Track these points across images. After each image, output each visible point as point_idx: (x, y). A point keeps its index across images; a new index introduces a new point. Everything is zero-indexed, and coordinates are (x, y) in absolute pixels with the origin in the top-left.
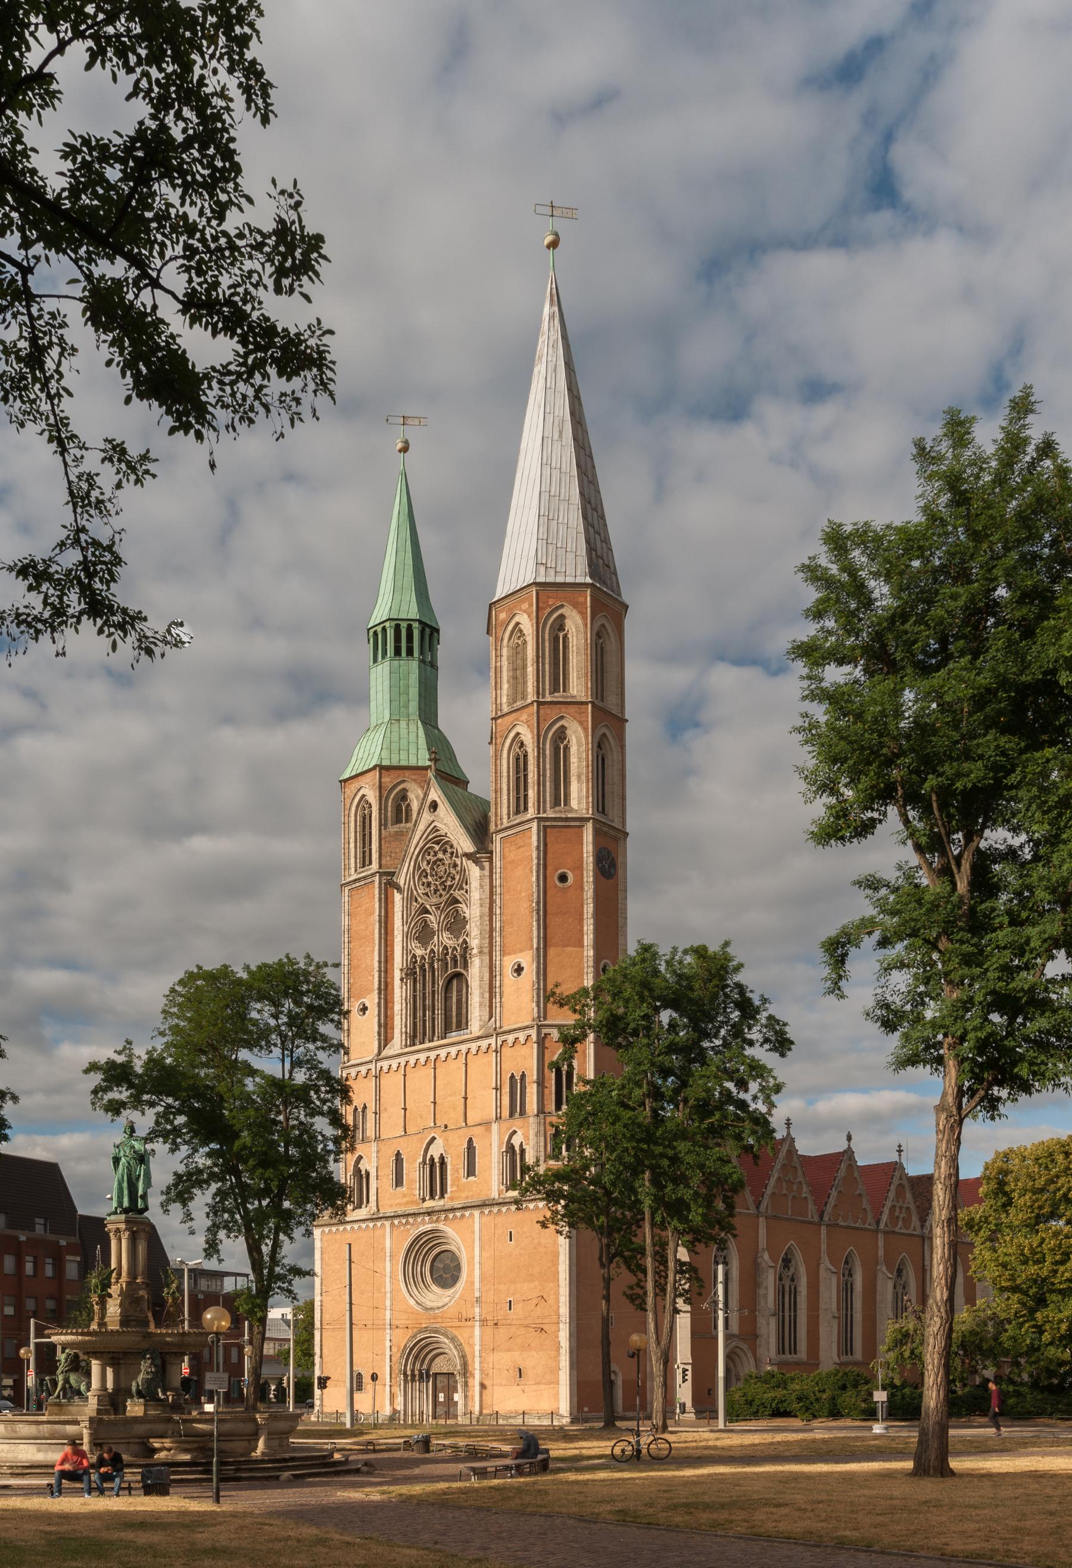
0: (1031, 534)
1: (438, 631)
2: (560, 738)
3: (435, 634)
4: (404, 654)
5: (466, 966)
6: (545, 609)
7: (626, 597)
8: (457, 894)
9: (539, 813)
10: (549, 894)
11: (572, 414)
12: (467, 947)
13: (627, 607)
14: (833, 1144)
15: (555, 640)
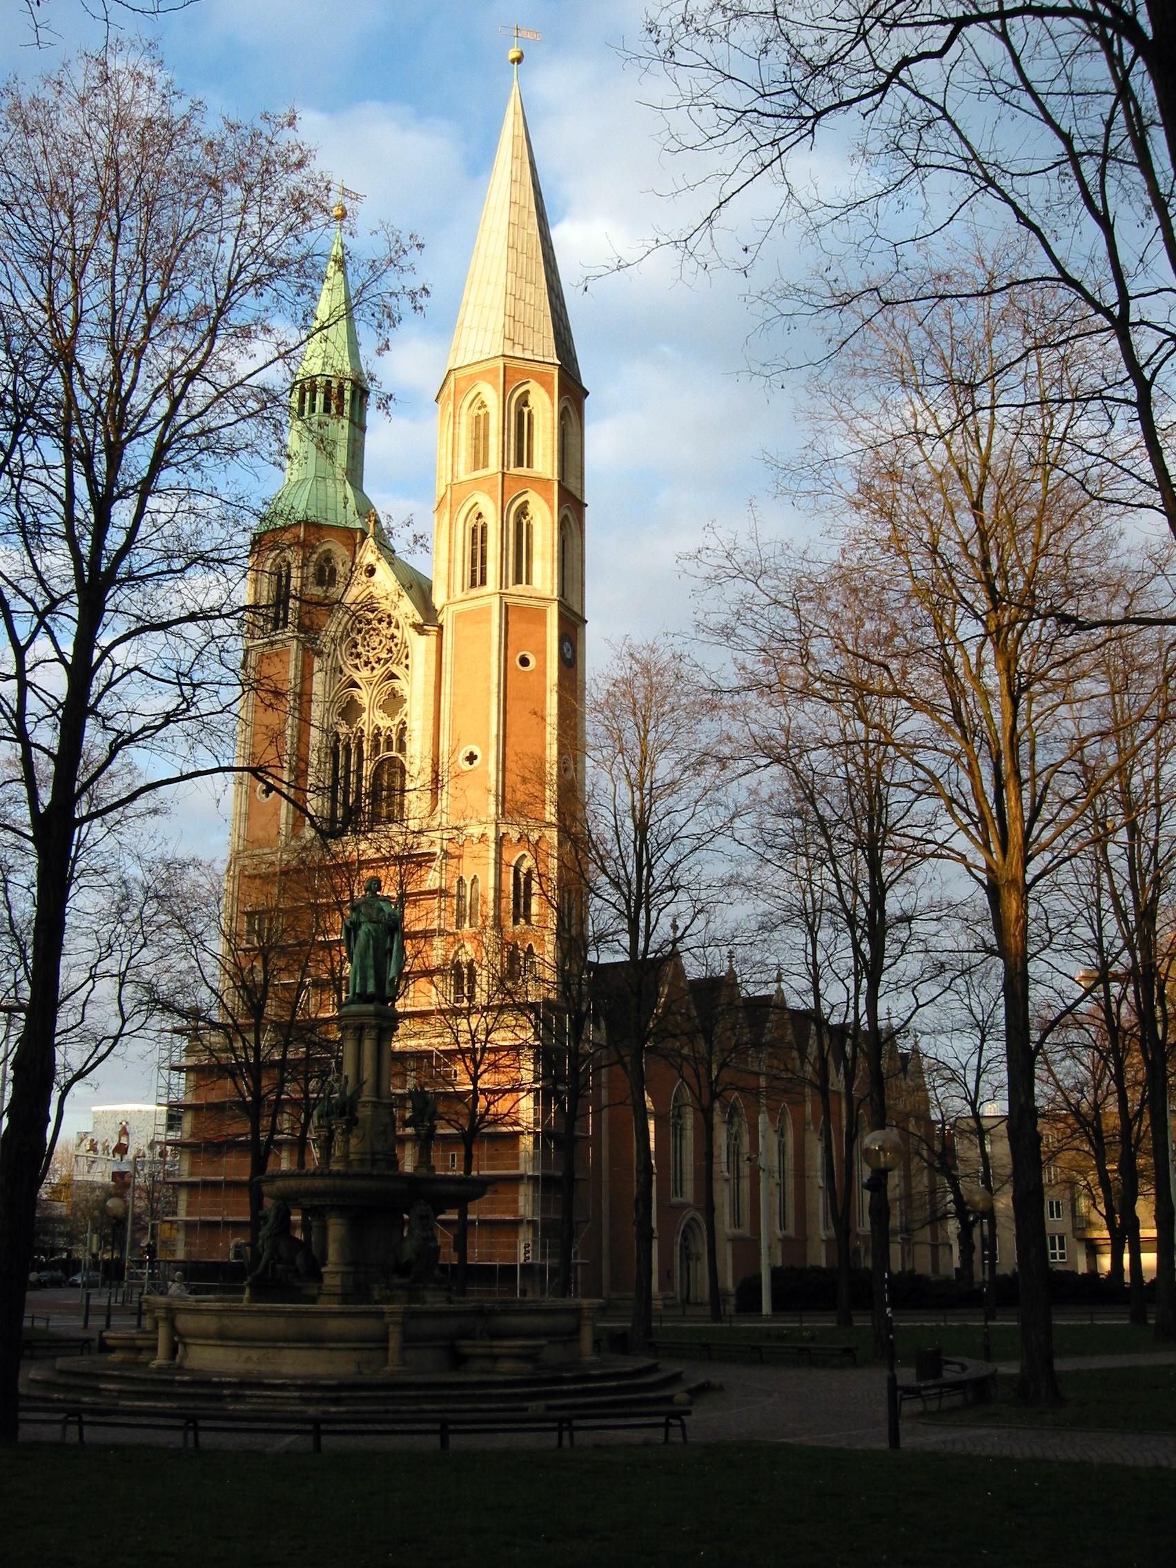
4: (333, 411)
5: (402, 748)
6: (512, 382)
7: (586, 384)
8: (395, 670)
10: (509, 677)
11: (537, 207)
14: (718, 962)
15: (520, 415)
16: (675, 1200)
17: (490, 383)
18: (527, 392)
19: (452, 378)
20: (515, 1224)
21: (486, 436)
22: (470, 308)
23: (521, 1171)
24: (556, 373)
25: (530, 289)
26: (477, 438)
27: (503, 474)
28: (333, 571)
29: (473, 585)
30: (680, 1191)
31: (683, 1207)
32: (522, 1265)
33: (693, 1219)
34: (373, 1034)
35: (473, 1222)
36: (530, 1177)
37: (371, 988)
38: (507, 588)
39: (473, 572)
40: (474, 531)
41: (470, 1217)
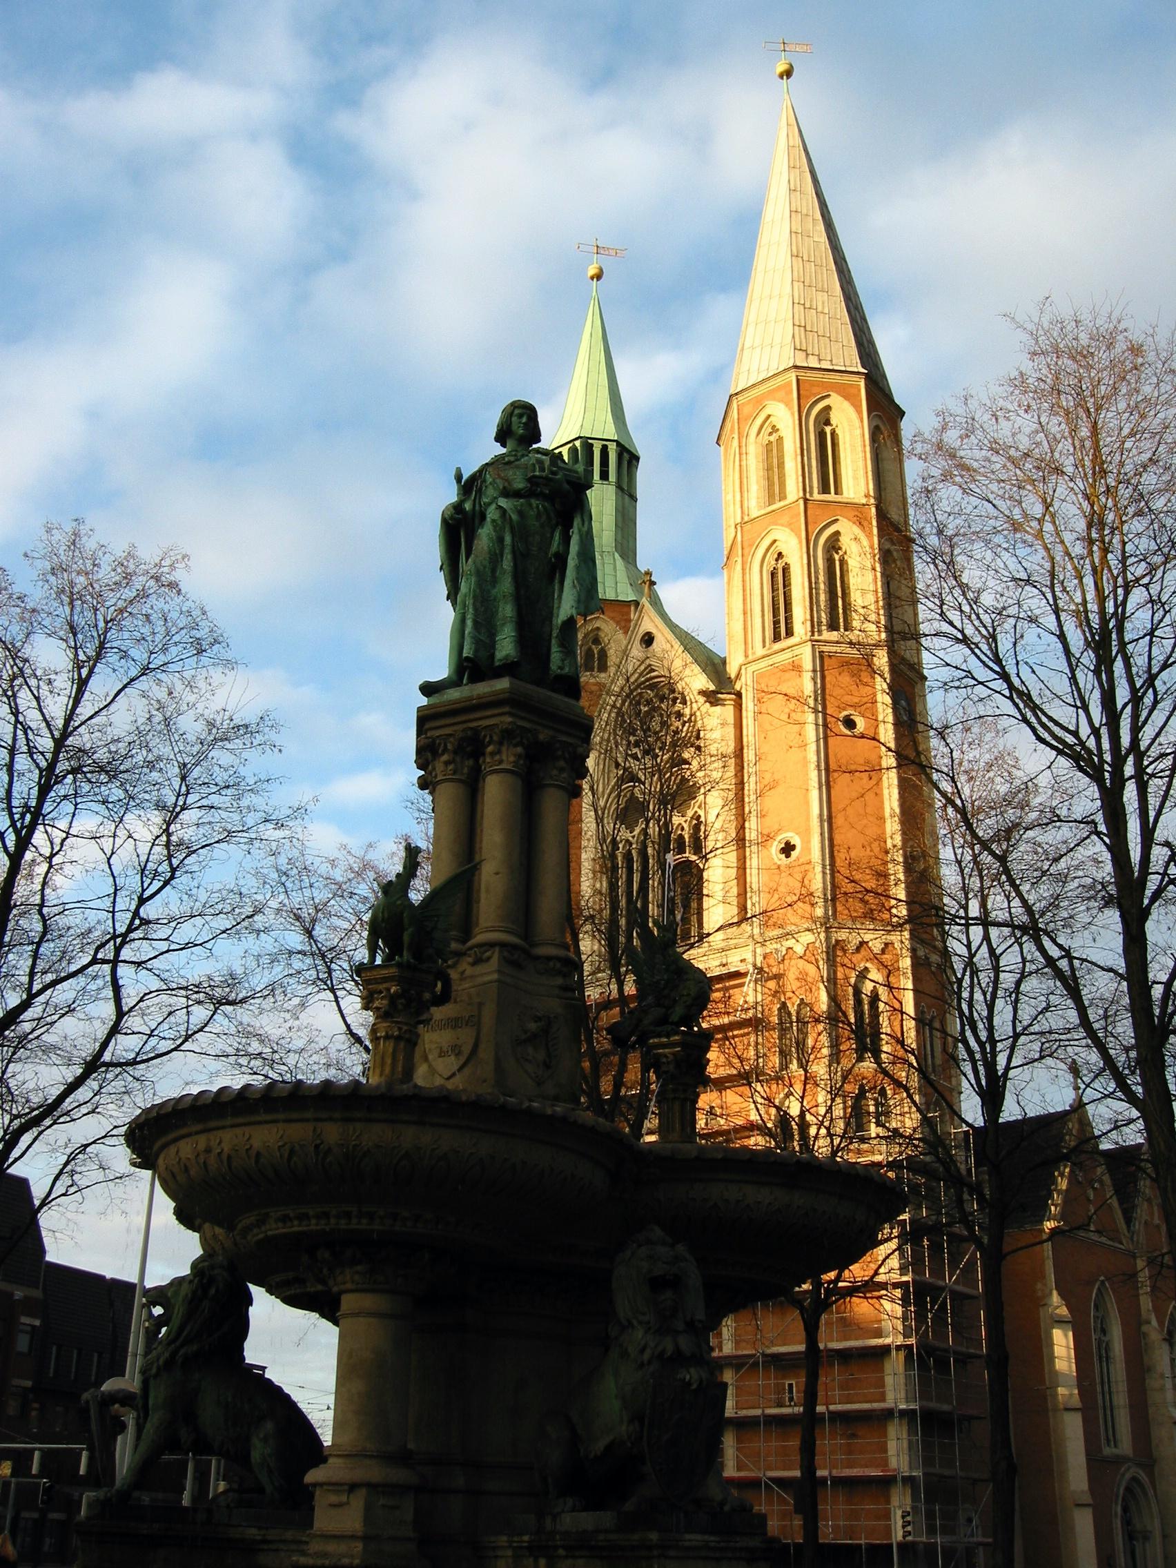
0: (890, 971)
1: (637, 459)
2: (834, 547)
3: (634, 462)
6: (808, 397)
9: (813, 635)
12: (700, 823)
13: (904, 413)
15: (821, 436)
16: (1108, 1451)
17: (781, 401)
18: (828, 408)
19: (735, 405)
20: (885, 1483)
21: (781, 465)
22: (751, 329)
23: (889, 1404)
24: (862, 384)
25: (822, 297)
26: (769, 469)
27: (806, 500)
28: (603, 655)
29: (777, 638)
30: (1113, 1440)
31: (1118, 1461)
32: (900, 1545)
33: (1134, 1479)
34: (509, 757)
35: (824, 1480)
36: (903, 1413)
37: (506, 646)
38: (820, 632)
39: (776, 623)
40: (773, 575)
41: (821, 1473)
